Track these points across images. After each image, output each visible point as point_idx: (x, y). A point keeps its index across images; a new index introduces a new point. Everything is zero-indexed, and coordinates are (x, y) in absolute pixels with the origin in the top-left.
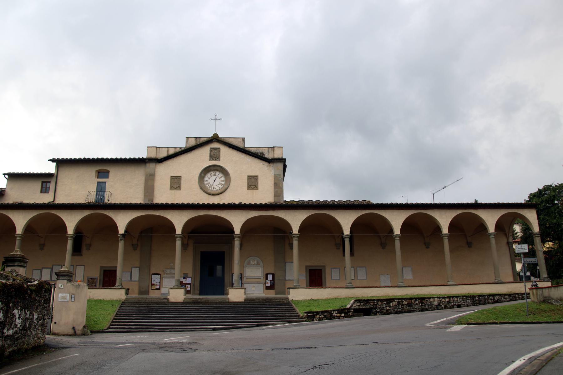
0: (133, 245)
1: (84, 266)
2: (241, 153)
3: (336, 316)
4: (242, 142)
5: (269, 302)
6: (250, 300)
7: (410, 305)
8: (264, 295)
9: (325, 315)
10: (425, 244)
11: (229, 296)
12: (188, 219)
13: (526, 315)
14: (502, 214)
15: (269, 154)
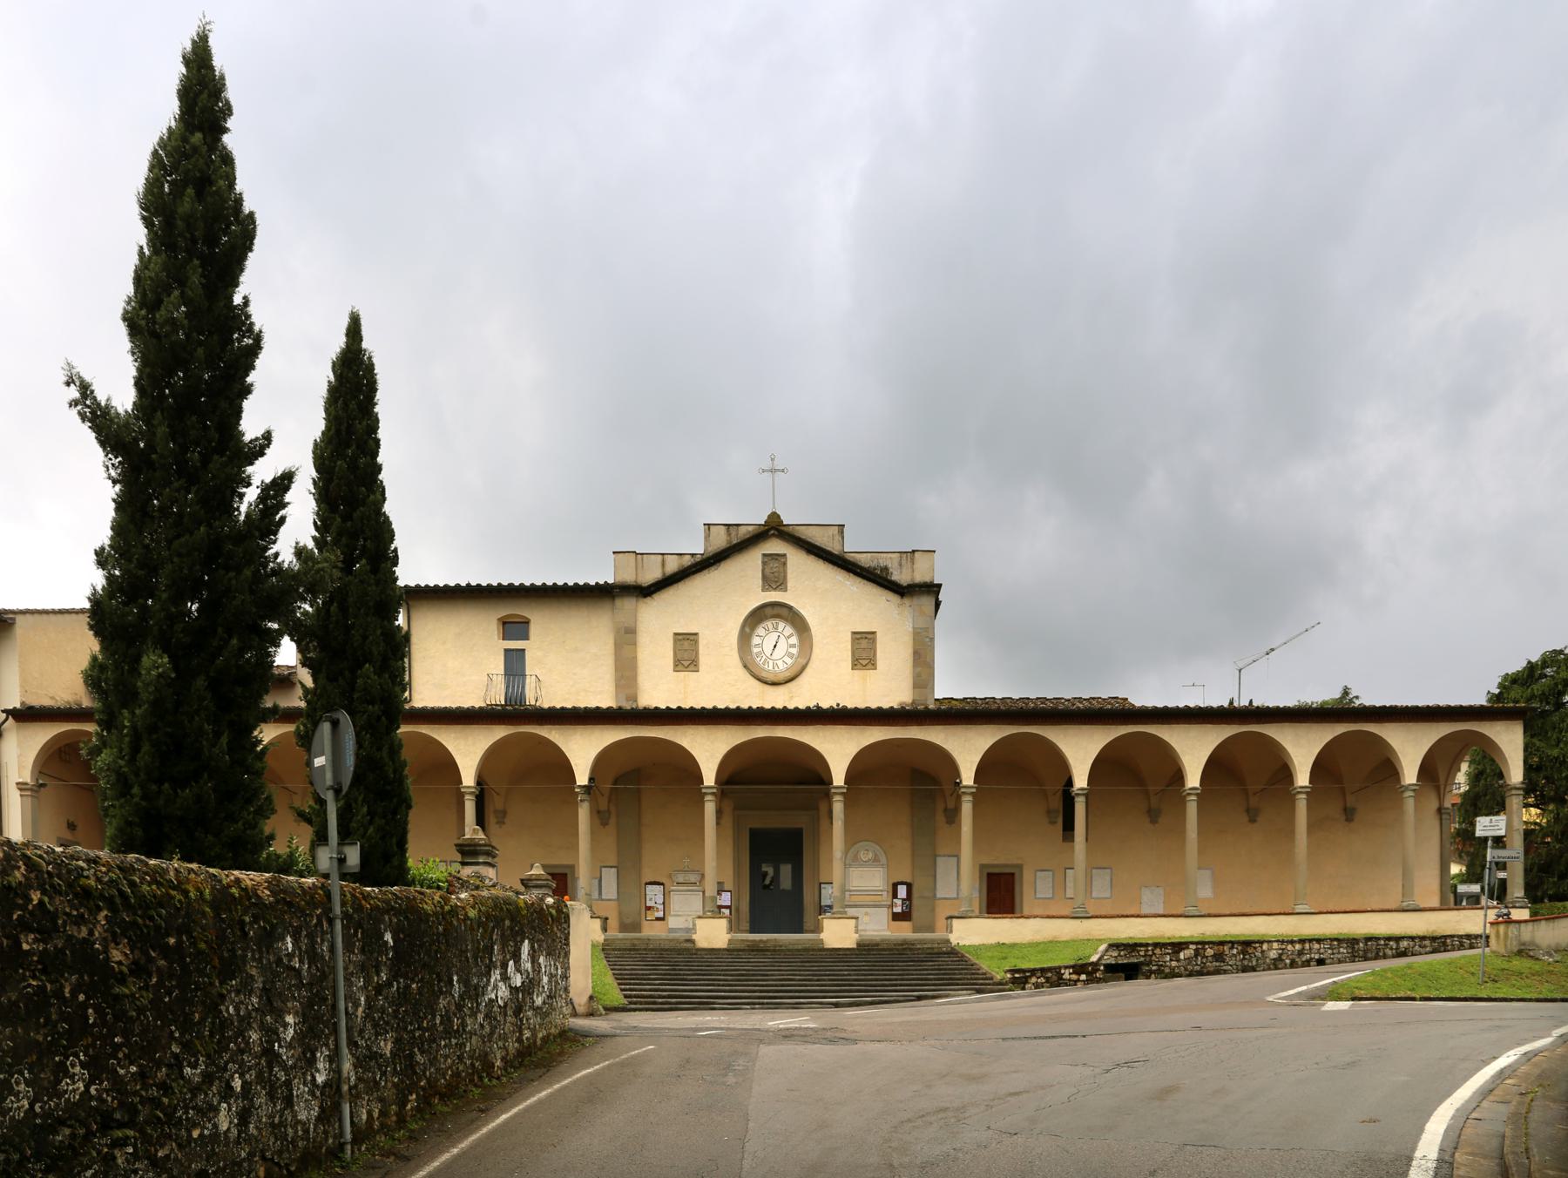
0: (599, 812)
1: (1111, 868)
2: (836, 568)
3: (1070, 980)
4: (838, 538)
6: (868, 945)
7: (1219, 957)
8: (888, 933)
10: (1248, 811)
11: (822, 936)
13: (1478, 984)
14: (1440, 736)
15: (901, 572)
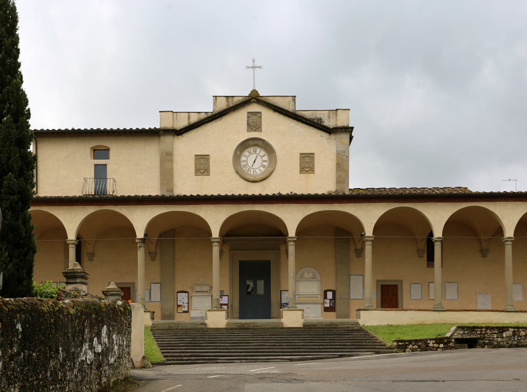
0: (150, 253)
3: (433, 347)
4: (292, 103)
5: (335, 328)
9: (419, 345)
11: (282, 320)
12: (227, 218)
15: (329, 121)
